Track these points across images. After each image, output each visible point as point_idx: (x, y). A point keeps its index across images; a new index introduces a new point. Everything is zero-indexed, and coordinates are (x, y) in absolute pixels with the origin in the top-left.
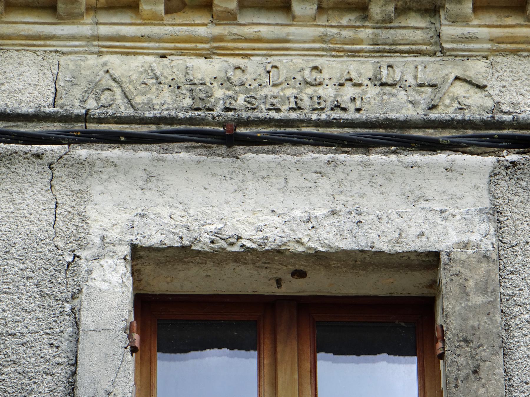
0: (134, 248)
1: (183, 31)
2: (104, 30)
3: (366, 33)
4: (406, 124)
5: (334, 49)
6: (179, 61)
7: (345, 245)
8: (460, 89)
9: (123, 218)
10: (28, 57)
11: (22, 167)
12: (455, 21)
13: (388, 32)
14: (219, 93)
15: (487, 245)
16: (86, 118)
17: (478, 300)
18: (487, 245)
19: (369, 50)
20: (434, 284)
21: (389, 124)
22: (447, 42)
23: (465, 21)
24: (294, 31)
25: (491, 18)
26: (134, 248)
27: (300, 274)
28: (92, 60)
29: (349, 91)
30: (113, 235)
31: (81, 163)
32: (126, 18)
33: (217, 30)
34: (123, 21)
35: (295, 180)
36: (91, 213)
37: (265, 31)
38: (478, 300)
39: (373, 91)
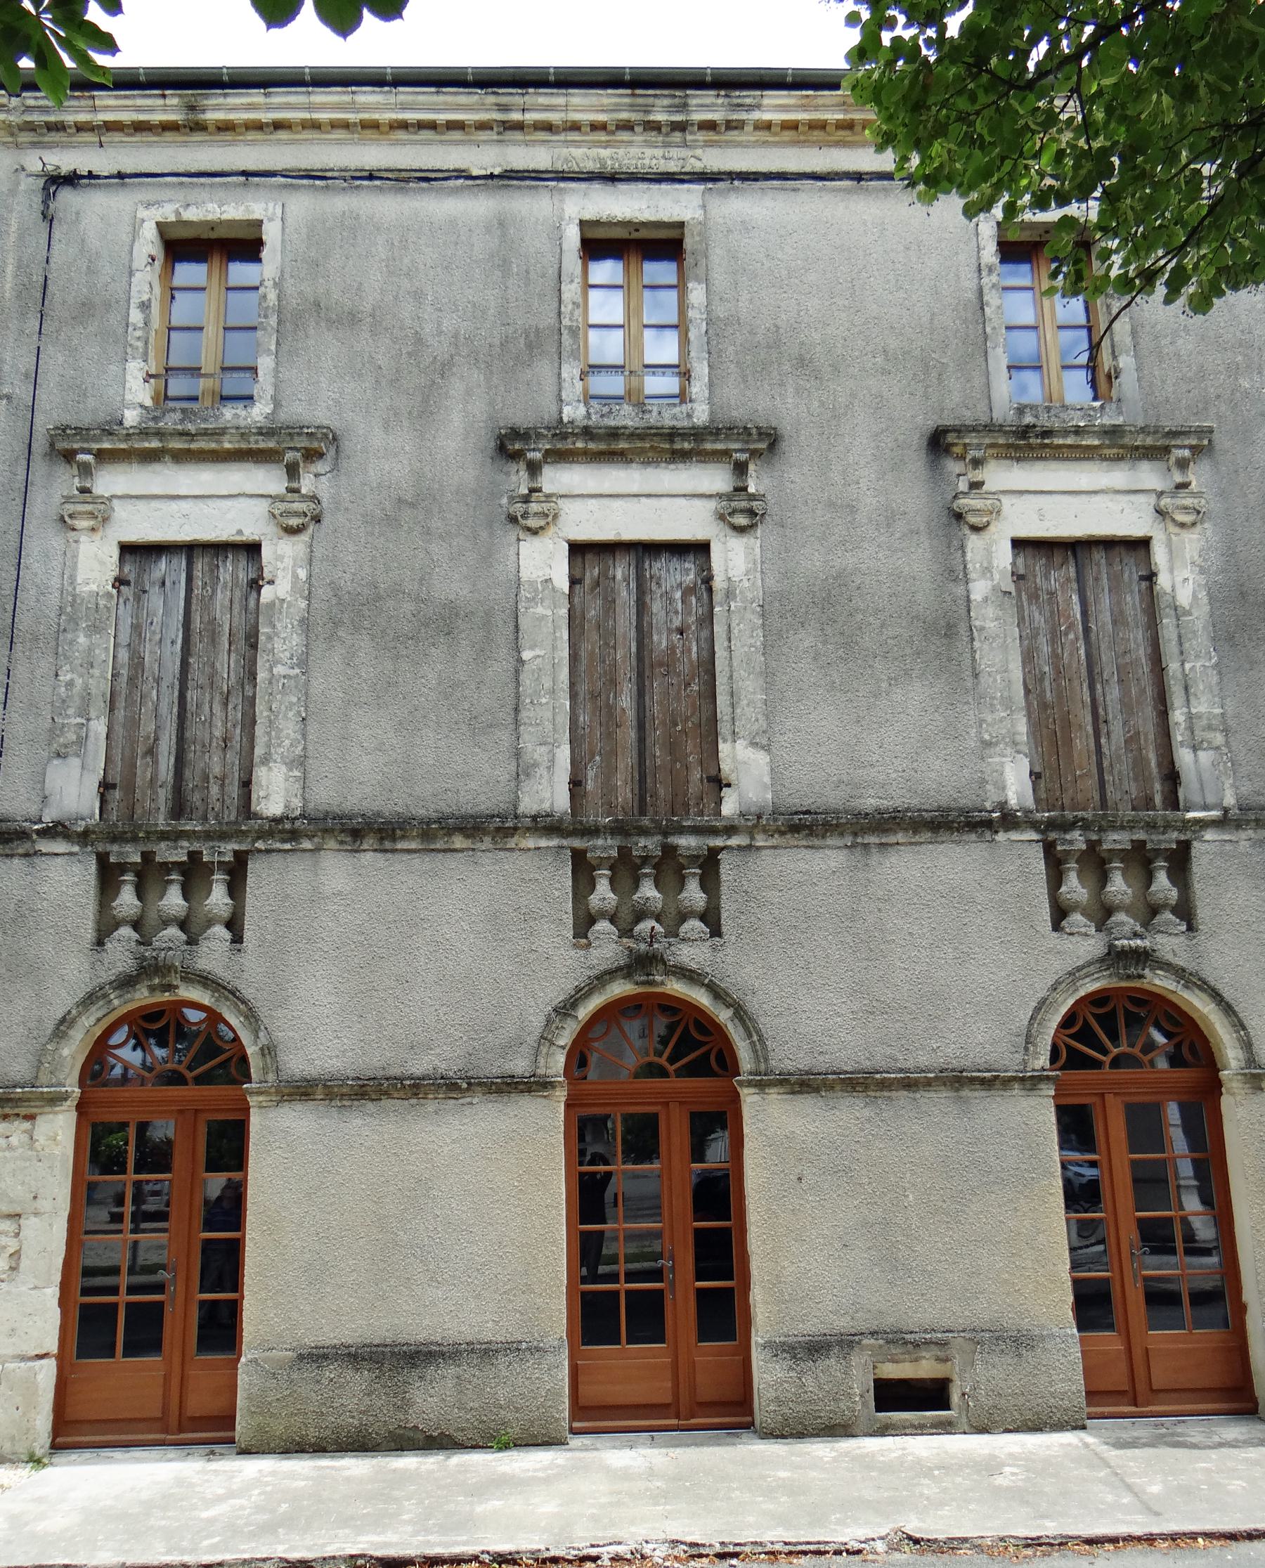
0: (581, 221)
1: (596, 138)
2: (569, 138)
3: (660, 139)
4: (674, 173)
5: (1149, 628)
6: (596, 150)
7: (653, 219)
8: (693, 160)
9: (576, 209)
10: (543, 149)
11: (541, 191)
12: (691, 133)
13: (225, 273)
14: (609, 162)
15: (701, 218)
16: (563, 172)
17: (697, 239)
18: (701, 218)
19: (50, 148)
20: (683, 234)
21: (668, 173)
22: (865, 124)
23: (695, 134)
24: (635, 138)
25: (704, 132)
26: (581, 221)
27: (637, 230)
28: (565, 150)
29: (654, 161)
30: (573, 216)
31: (561, 189)
32: (577, 133)
33: (608, 138)
34: (792, 166)
35: (635, 195)
36: (565, 207)
37: (625, 138)
38: (697, 239)
39: (662, 161)
